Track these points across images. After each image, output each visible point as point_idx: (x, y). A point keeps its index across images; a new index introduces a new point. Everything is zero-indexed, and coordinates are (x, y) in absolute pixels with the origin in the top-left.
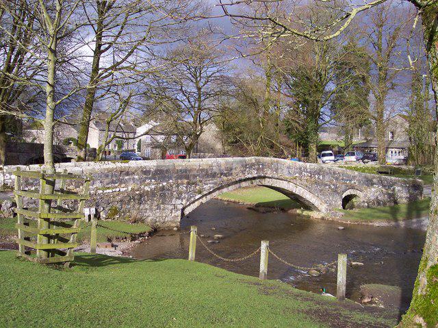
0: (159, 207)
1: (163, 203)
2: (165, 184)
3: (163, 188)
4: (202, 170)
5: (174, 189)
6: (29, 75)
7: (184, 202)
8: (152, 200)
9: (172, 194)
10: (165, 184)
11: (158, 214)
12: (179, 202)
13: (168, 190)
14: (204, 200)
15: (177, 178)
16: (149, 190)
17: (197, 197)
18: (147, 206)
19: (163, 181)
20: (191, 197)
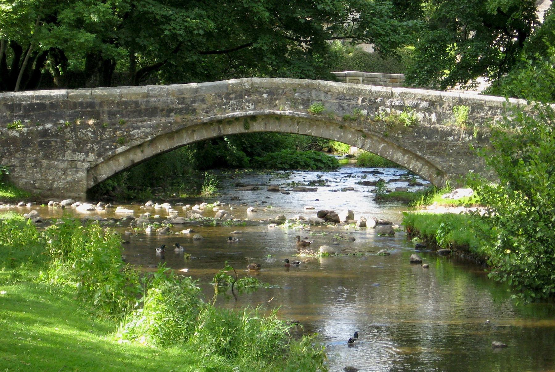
0: (37, 163)
1: (46, 157)
2: (49, 126)
3: (45, 133)
4: (126, 103)
5: (68, 135)
6: (25, 272)
7: (92, 157)
8: (25, 151)
9: (64, 143)
10: (49, 126)
11: (38, 176)
12: (82, 156)
13: (56, 136)
14: (138, 156)
15: (73, 118)
16: (17, 135)
17: (120, 150)
18: (14, 161)
19: (47, 123)
20: (107, 150)
